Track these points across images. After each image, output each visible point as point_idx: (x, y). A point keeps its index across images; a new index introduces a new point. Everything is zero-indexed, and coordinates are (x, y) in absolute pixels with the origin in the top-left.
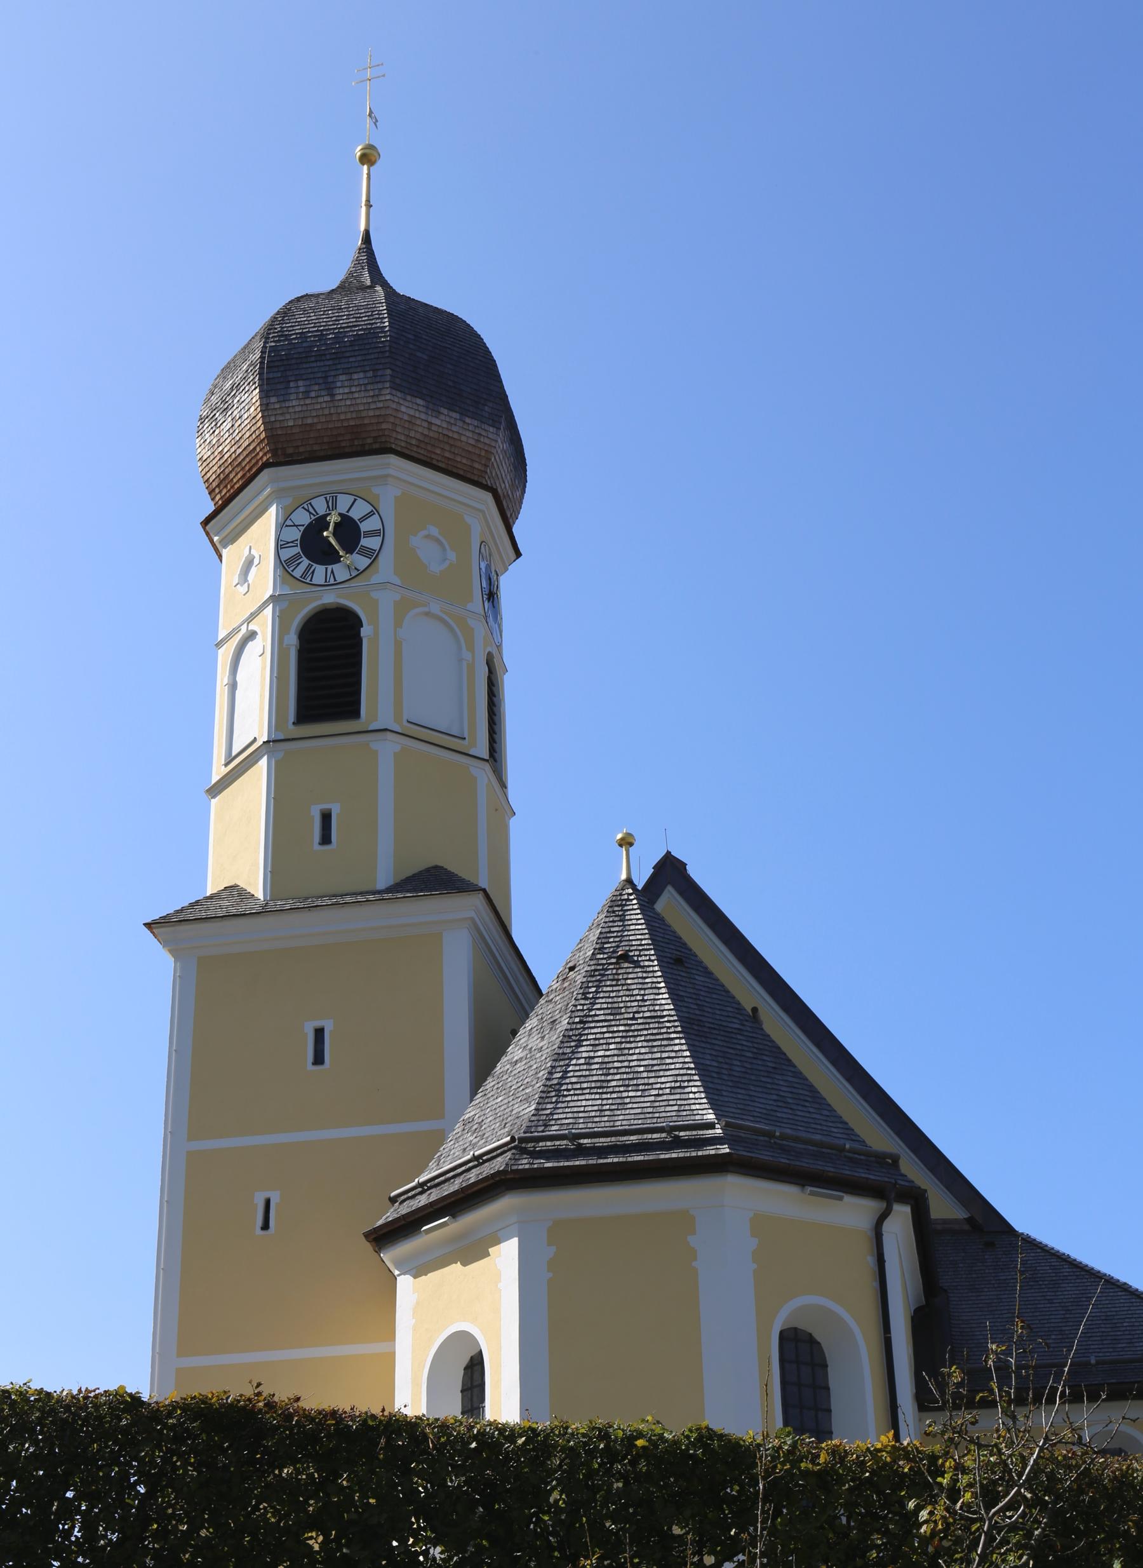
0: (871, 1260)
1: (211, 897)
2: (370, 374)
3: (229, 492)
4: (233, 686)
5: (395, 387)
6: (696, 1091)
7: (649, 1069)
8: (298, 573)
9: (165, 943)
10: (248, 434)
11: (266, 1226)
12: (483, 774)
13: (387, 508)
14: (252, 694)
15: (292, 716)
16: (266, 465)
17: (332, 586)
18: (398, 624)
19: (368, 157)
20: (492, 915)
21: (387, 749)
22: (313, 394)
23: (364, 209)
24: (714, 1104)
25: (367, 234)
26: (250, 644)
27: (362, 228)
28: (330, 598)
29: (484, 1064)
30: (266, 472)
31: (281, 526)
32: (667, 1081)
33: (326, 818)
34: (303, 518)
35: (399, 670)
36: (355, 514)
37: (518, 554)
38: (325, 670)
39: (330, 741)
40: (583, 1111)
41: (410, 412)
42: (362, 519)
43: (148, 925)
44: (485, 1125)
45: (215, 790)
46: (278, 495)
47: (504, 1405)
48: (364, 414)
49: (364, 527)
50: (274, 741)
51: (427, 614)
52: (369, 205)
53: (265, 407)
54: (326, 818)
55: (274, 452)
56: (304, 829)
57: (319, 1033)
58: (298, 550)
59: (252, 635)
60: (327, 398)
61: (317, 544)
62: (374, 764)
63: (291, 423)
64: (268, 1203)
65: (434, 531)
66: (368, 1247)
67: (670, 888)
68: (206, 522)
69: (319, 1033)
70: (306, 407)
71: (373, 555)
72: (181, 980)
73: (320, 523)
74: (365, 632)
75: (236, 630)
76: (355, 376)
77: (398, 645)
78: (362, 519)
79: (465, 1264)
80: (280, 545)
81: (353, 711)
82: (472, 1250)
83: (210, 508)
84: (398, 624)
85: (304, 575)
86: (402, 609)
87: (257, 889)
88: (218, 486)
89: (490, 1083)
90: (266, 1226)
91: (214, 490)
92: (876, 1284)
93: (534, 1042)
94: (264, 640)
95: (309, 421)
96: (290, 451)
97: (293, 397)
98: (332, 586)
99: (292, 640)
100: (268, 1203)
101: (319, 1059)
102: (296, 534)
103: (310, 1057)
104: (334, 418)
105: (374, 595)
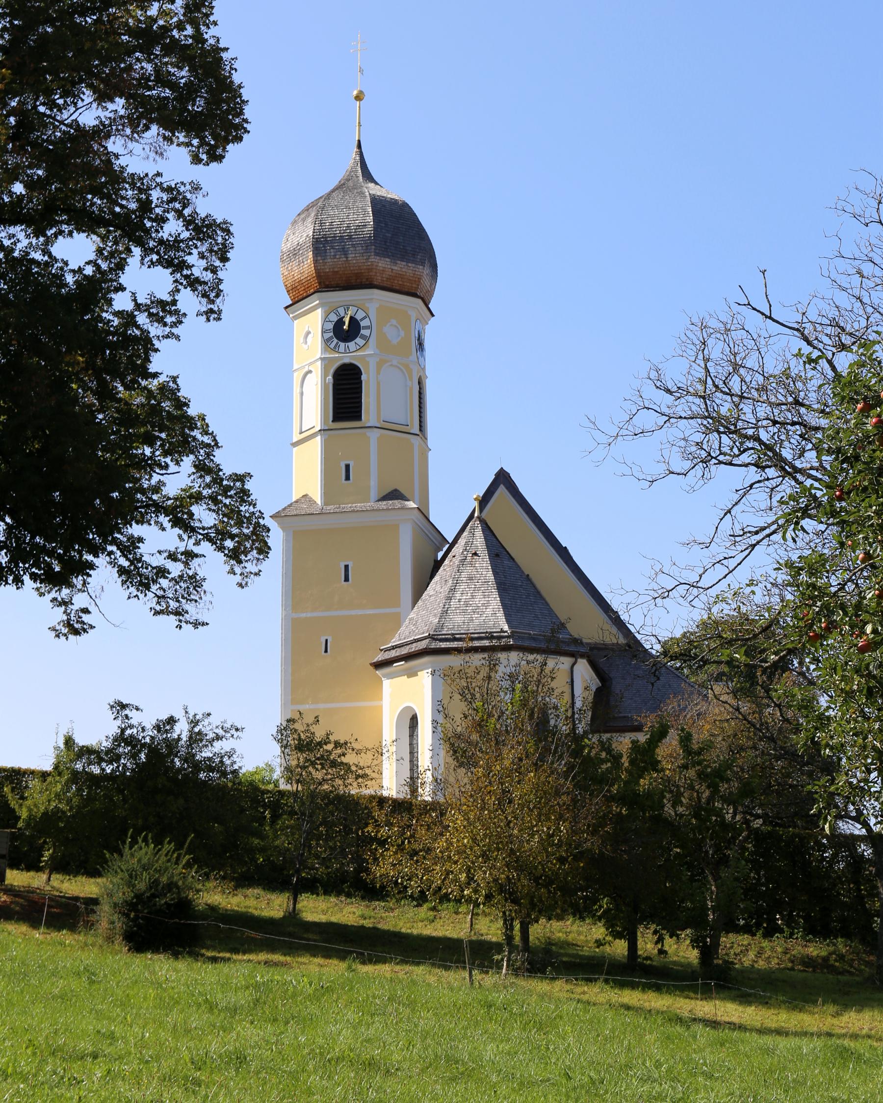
1: (296, 502)
3: (299, 295)
4: (302, 394)
5: (377, 254)
6: (501, 615)
7: (483, 605)
8: (332, 346)
11: (326, 651)
13: (373, 314)
14: (311, 402)
15: (331, 419)
18: (378, 373)
19: (358, 98)
20: (421, 515)
24: (508, 621)
25: (359, 141)
29: (419, 591)
31: (325, 320)
32: (489, 611)
34: (334, 318)
35: (378, 398)
36: (358, 317)
37: (433, 315)
38: (346, 394)
39: (348, 431)
40: (457, 622)
41: (383, 265)
42: (361, 320)
44: (417, 622)
45: (295, 444)
47: (426, 794)
49: (362, 324)
50: (324, 430)
51: (391, 365)
52: (360, 125)
53: (315, 262)
55: (320, 283)
56: (340, 473)
57: (347, 567)
58: (332, 334)
59: (310, 372)
61: (344, 332)
62: (367, 442)
64: (327, 641)
65: (394, 322)
66: (372, 668)
69: (347, 567)
70: (333, 262)
71: (366, 339)
73: (340, 322)
74: (363, 377)
75: (304, 367)
78: (361, 320)
81: (358, 417)
82: (412, 674)
83: (291, 302)
84: (378, 373)
85: (335, 347)
86: (380, 365)
87: (317, 496)
89: (420, 603)
90: (326, 651)
93: (438, 588)
99: (330, 378)
100: (327, 641)
101: (348, 478)
102: (331, 326)
103: (343, 578)
105: (368, 359)
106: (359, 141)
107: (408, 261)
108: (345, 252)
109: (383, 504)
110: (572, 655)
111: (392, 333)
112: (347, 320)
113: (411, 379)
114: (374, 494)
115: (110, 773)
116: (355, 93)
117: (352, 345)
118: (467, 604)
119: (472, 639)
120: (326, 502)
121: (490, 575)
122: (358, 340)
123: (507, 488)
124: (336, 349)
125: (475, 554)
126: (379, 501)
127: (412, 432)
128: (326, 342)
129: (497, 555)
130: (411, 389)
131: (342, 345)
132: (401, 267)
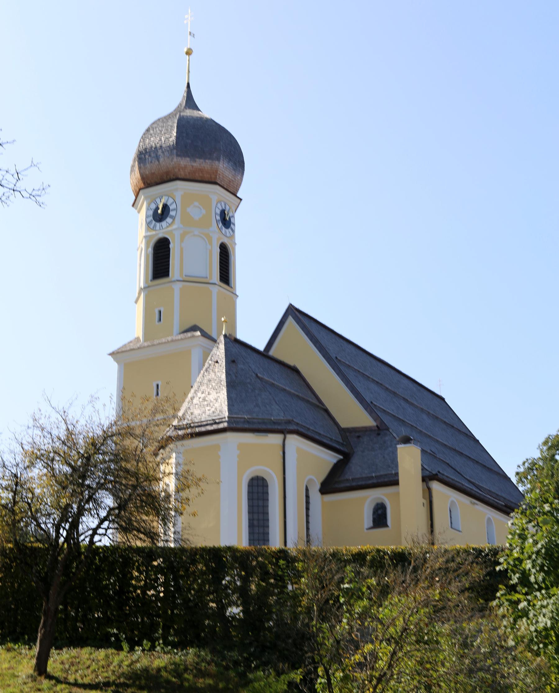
0: (281, 453)
5: (178, 155)
9: (115, 359)
12: (217, 289)
16: (140, 189)
17: (163, 230)
21: (177, 287)
25: (188, 84)
30: (141, 192)
31: (148, 209)
34: (153, 206)
37: (241, 200)
43: (112, 354)
49: (171, 208)
55: (144, 183)
56: (155, 317)
61: (161, 215)
65: (196, 204)
68: (133, 205)
70: (152, 167)
71: (173, 218)
72: (119, 371)
74: (171, 246)
77: (182, 250)
80: (147, 217)
84: (182, 240)
86: (183, 236)
92: (282, 460)
98: (163, 230)
99: (150, 250)
102: (151, 213)
106: (188, 84)
107: (205, 158)
108: (157, 158)
109: (182, 336)
110: (283, 432)
111: (196, 212)
112: (161, 207)
113: (211, 243)
114: (176, 328)
115: (258, 590)
116: (185, 50)
117: (164, 224)
118: (204, 400)
119: (207, 425)
120: (145, 339)
121: (224, 376)
122: (169, 220)
123: (293, 318)
124: (154, 229)
125: (217, 362)
126: (180, 333)
127: (211, 281)
128: (148, 224)
129: (233, 361)
130: (211, 252)
131: (158, 224)
132: (199, 164)
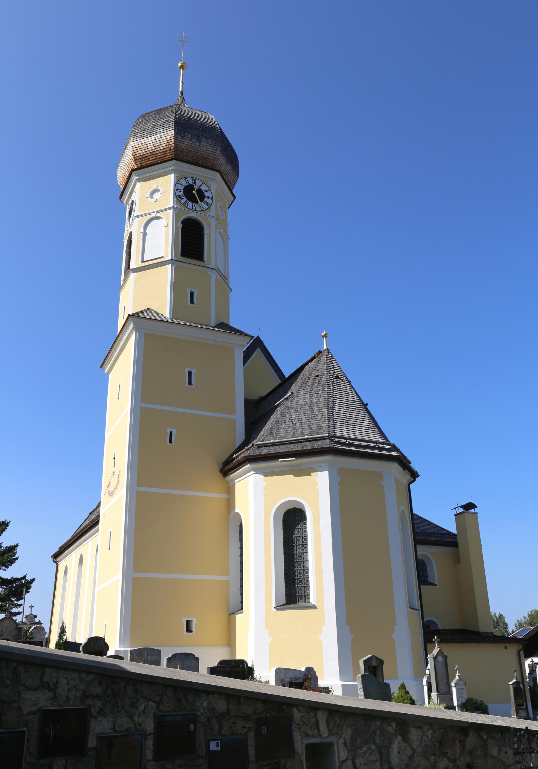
2: (214, 142)
10: (164, 145)
22: (193, 140)
23: (181, 84)
26: (155, 221)
27: (180, 90)
28: (193, 215)
30: (174, 161)
31: (176, 184)
33: (192, 294)
46: (175, 171)
48: (210, 155)
52: (183, 84)
53: (176, 138)
54: (192, 294)
55: (175, 155)
60: (198, 144)
61: (189, 194)
63: (184, 147)
67: (258, 348)
69: (190, 373)
76: (209, 140)
79: (296, 476)
80: (176, 190)
88: (141, 159)
91: (137, 159)
94: (167, 221)
95: (190, 149)
96: (181, 157)
97: (186, 138)
99: (180, 225)
104: (199, 152)
105: (209, 220)
